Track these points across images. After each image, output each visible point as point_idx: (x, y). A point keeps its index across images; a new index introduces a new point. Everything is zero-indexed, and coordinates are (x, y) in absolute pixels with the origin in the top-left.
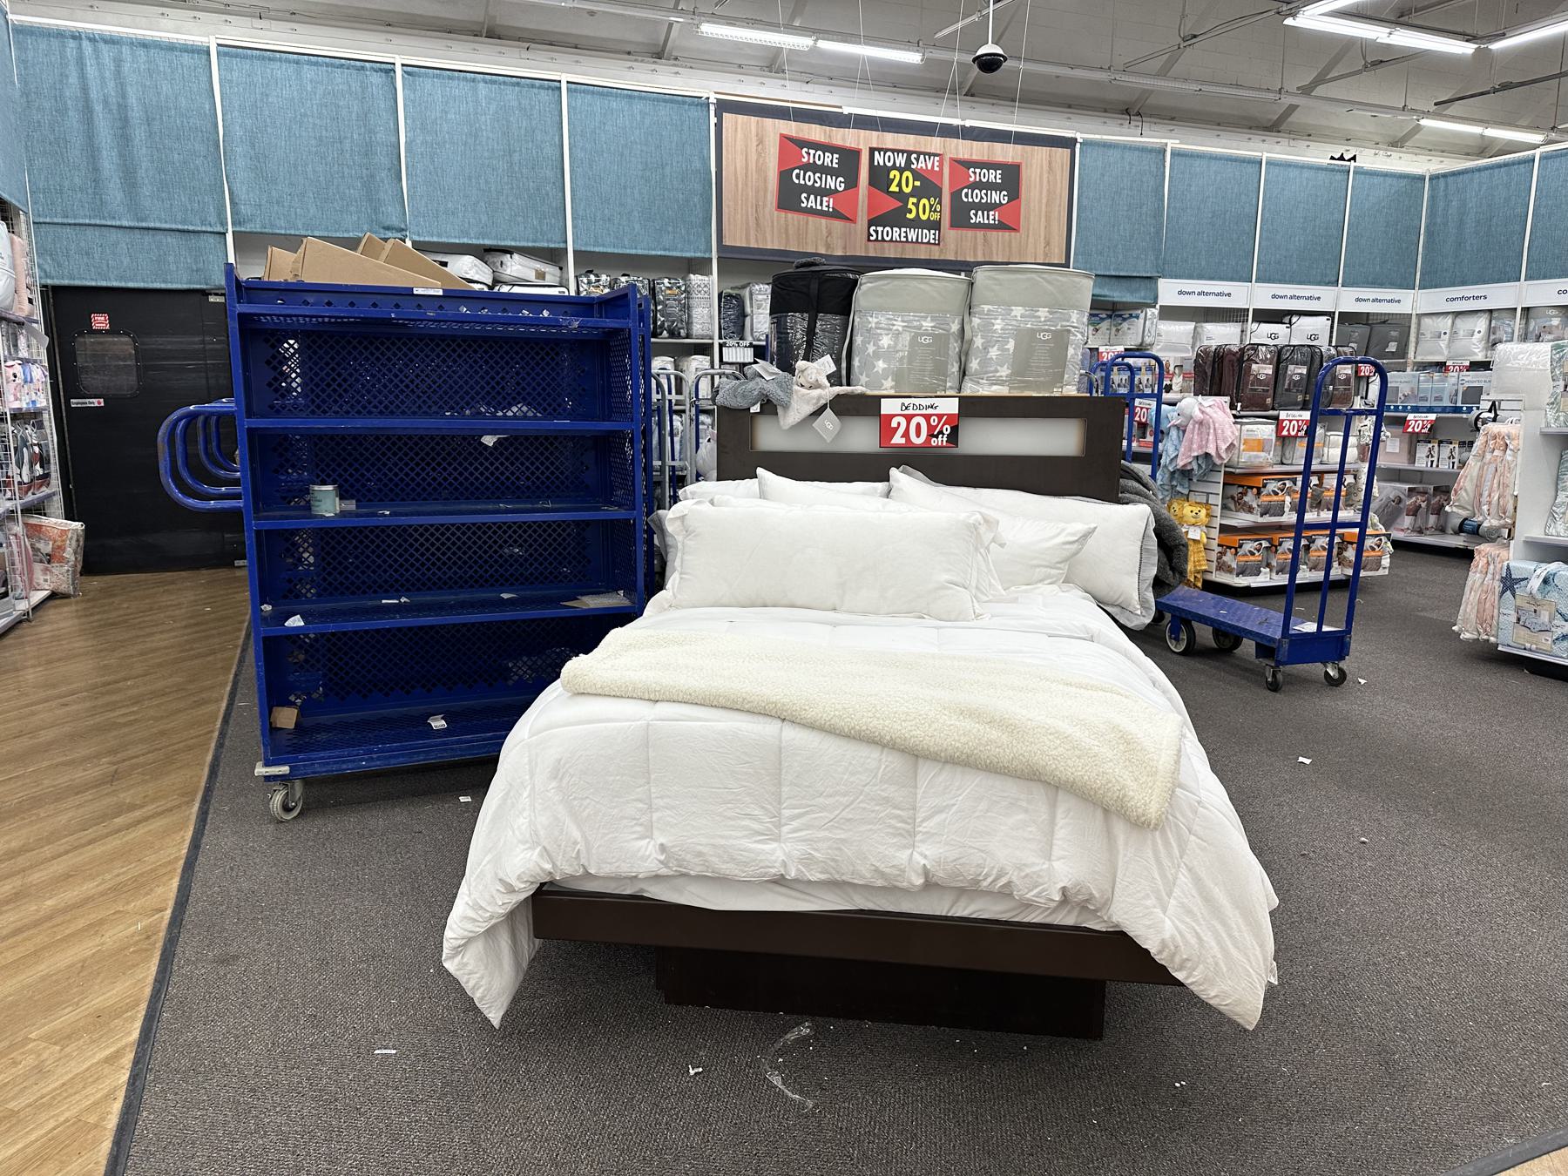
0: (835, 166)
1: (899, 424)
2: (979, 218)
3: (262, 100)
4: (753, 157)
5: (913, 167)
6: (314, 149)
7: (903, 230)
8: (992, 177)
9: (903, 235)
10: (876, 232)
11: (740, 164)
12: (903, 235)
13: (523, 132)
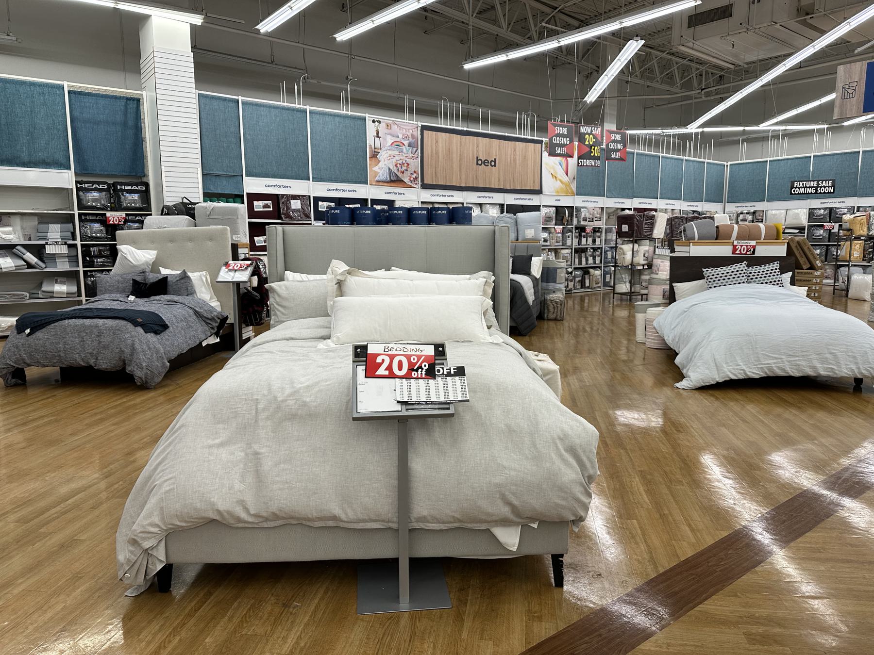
1: (383, 360)
3: (49, 141)
4: (434, 147)
6: (104, 136)
10: (581, 162)
11: (429, 152)
13: (290, 130)
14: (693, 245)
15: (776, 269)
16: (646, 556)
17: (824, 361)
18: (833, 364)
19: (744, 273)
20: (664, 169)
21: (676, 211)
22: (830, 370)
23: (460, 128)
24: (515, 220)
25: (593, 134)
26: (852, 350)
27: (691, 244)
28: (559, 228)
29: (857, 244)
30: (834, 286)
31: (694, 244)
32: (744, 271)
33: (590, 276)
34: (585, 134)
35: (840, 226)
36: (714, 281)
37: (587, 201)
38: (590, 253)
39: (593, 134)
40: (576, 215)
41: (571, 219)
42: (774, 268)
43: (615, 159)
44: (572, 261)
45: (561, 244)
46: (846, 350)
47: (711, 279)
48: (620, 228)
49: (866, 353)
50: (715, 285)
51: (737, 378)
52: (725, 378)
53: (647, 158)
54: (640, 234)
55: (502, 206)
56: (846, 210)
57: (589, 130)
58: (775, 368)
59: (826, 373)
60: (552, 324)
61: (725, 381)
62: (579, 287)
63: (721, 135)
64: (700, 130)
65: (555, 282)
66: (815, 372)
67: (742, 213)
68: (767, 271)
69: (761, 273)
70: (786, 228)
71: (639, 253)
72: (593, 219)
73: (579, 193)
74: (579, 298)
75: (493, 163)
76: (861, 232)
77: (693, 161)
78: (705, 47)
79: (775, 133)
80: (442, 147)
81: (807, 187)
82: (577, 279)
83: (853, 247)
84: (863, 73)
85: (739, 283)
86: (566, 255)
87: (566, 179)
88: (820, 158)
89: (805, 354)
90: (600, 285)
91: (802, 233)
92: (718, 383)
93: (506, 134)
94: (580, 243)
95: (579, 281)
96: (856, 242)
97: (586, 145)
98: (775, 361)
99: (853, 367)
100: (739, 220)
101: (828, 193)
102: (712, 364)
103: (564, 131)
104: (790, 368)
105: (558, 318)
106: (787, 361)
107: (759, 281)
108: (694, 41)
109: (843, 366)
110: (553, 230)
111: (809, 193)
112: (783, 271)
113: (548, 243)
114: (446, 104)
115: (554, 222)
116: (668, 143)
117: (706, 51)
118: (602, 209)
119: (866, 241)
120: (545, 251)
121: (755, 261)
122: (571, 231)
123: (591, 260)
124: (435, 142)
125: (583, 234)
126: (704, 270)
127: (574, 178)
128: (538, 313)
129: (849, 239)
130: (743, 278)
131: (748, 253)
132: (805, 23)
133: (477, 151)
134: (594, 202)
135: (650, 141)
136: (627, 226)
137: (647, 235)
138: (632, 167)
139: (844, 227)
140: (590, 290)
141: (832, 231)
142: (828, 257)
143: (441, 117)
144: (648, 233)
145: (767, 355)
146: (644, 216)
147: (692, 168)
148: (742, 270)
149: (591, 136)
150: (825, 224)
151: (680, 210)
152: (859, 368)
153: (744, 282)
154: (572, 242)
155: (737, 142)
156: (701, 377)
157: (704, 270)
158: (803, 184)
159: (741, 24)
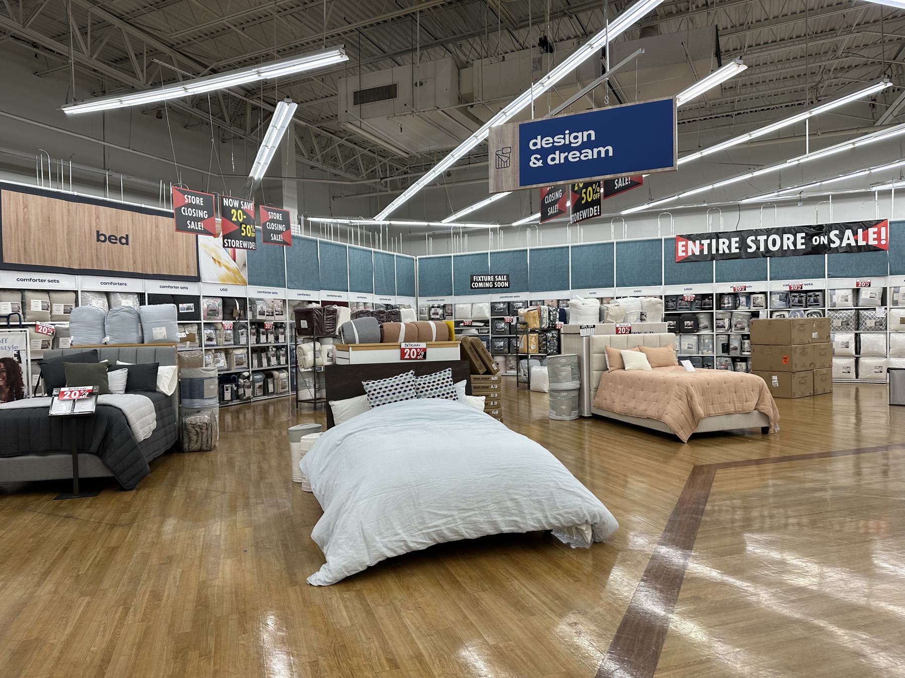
0: (202, 204)
2: (192, 226)
5: (242, 208)
7: (241, 241)
8: (198, 201)
9: (241, 244)
10: (228, 242)
12: (241, 244)
14: (352, 350)
15: (448, 378)
16: (403, 614)
17: (505, 511)
18: (516, 515)
19: (412, 385)
20: (352, 259)
21: (368, 305)
22: (513, 524)
23: (71, 192)
24: (136, 315)
25: (242, 210)
26: (535, 492)
27: (350, 348)
28: (229, 323)
29: (532, 336)
30: (517, 376)
31: (354, 348)
32: (412, 383)
33: (274, 379)
34: (230, 208)
35: (518, 318)
36: (377, 398)
37: (303, 294)
38: (273, 353)
39: (242, 210)
40: (251, 308)
41: (245, 313)
42: (446, 377)
43: (275, 242)
44: (248, 363)
45: (232, 342)
46: (528, 493)
47: (373, 394)
48: (298, 323)
49: (552, 494)
50: (378, 403)
51: (395, 555)
52: (378, 558)
53: (333, 248)
54: (321, 330)
55: (141, 296)
56: (521, 304)
57: (236, 204)
58: (446, 532)
59: (508, 529)
60: (193, 457)
61: (380, 562)
62: (261, 394)
63: (410, 229)
64: (387, 223)
65: (202, 397)
66: (496, 529)
67: (433, 307)
68: (439, 380)
69: (432, 384)
70: (473, 321)
71: (322, 353)
72: (273, 313)
73: (252, 283)
74: (261, 407)
75: (124, 241)
76: (535, 325)
77: (383, 254)
78: (374, 128)
79: (456, 231)
80: (107, 225)
81: (485, 282)
82: (257, 385)
83: (529, 340)
84: (516, 137)
85: (407, 399)
86: (240, 356)
87: (233, 265)
88: (496, 255)
89: (481, 504)
90: (287, 389)
91: (487, 326)
92: (369, 567)
93: (143, 206)
94: (258, 341)
95: (260, 387)
96: (532, 335)
97: (234, 222)
98: (444, 521)
99: (539, 515)
100: (431, 314)
101: (504, 287)
102: (360, 539)
103: (199, 201)
104: (464, 527)
105: (204, 447)
106: (460, 518)
107: (430, 394)
108: (361, 120)
109: (528, 517)
110: (220, 326)
111: (487, 288)
112: (456, 380)
113: (214, 342)
114: (46, 160)
115: (221, 316)
116: (356, 234)
117: (377, 134)
118: (284, 301)
119: (539, 334)
120: (210, 353)
121: (424, 368)
122: (245, 327)
123: (274, 361)
124: (94, 217)
125: (262, 330)
126: (364, 383)
127: (244, 265)
128: (174, 442)
129: (525, 332)
130: (411, 392)
131: (418, 357)
132: (465, 111)
133: (156, 232)
134: (339, 296)
135: (336, 230)
136: (305, 322)
137: (330, 332)
138: (316, 257)
139: (520, 320)
140: (275, 396)
141: (512, 324)
142: (511, 349)
143: (40, 177)
144: (331, 330)
145: (434, 513)
146: (324, 310)
147: (382, 261)
148: (409, 382)
149: (240, 211)
150: (505, 317)
151: (373, 304)
152: (546, 517)
153: (412, 397)
154: (248, 340)
155: (423, 238)
156: (344, 563)
157: (364, 383)
158: (481, 278)
159: (405, 105)
